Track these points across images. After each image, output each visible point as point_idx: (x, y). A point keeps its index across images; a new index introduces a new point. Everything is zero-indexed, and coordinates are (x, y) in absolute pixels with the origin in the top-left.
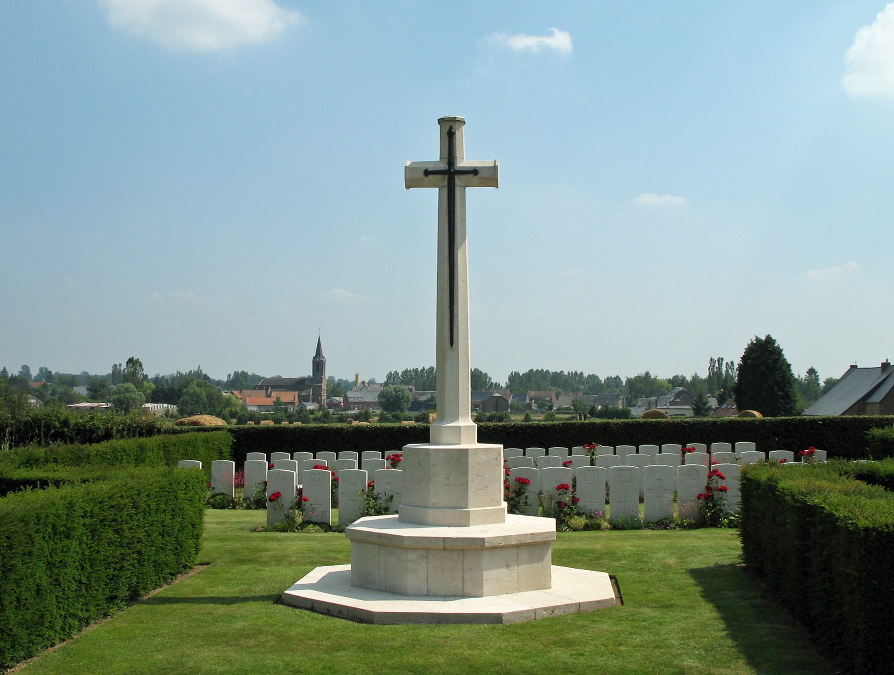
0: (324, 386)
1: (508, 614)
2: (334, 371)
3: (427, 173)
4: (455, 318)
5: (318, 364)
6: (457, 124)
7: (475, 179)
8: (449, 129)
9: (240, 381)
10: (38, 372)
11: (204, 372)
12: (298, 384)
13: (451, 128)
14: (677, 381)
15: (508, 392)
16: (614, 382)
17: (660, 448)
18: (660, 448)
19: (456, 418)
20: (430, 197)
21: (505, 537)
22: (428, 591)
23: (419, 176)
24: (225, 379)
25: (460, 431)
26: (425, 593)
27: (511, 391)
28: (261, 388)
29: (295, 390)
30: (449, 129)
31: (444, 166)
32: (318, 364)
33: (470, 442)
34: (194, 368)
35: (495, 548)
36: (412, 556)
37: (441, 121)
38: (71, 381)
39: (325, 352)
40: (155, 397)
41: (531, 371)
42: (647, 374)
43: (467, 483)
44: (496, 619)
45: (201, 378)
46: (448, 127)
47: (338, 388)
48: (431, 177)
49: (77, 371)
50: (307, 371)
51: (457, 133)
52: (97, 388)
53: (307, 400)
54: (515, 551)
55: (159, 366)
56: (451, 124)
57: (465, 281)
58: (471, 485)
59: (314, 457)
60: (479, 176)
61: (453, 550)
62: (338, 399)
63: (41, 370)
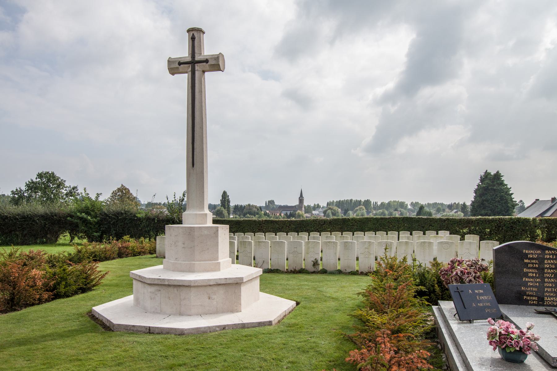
5: (301, 200)
30: (195, 35)
32: (301, 200)
48: (182, 66)
56: (193, 32)
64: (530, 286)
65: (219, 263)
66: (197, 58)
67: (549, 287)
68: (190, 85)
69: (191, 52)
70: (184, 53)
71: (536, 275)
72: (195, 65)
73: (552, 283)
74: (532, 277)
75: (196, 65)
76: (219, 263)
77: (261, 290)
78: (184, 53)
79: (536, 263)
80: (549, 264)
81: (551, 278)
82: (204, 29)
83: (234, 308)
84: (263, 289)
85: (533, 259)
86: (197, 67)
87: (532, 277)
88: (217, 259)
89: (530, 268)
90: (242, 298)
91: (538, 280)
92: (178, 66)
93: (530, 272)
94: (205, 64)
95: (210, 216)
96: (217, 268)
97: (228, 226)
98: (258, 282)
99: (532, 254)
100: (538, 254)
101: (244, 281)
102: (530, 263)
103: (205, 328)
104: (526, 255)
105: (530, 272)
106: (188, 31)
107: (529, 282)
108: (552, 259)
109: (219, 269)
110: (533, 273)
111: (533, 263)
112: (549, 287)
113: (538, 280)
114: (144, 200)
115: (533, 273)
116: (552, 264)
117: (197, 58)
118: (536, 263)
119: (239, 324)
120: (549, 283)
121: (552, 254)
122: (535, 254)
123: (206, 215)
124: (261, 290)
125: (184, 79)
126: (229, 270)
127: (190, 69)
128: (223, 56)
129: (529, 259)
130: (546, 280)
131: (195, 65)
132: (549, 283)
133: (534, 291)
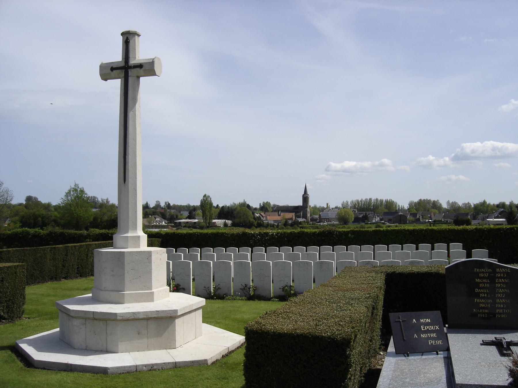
0: (308, 210)
1: (113, 368)
2: (312, 203)
3: (112, 69)
4: (127, 164)
5: (305, 199)
6: (131, 35)
7: (141, 71)
8: (128, 38)
9: (265, 208)
10: (408, 206)
11: (247, 203)
12: (295, 209)
13: (127, 39)
14: (502, 205)
15: (408, 212)
16: (468, 205)
17: (402, 247)
18: (402, 247)
19: (127, 232)
20: (115, 85)
21: (134, 313)
22: (86, 347)
23: (108, 72)
24: (258, 207)
25: (134, 238)
26: (85, 348)
27: (409, 212)
28: (275, 211)
29: (293, 212)
30: (128, 38)
31: (123, 64)
32: (305, 199)
33: (144, 247)
34: (242, 201)
35: (128, 320)
36: (76, 322)
37: (123, 34)
38: (179, 208)
39: (309, 192)
40: (219, 217)
41: (420, 200)
42: (484, 201)
43: (124, 274)
44: (103, 371)
45: (245, 206)
46: (126, 38)
47: (315, 210)
48: (114, 71)
49: (184, 203)
50: (299, 202)
51: (131, 41)
52: (192, 211)
53: (300, 217)
54: (145, 322)
55: (220, 200)
56: (127, 35)
57: (135, 140)
58: (127, 275)
59: (176, 252)
60: (143, 69)
61: (100, 320)
62: (316, 216)
63: (166, 203)
64: (482, 308)
65: (153, 293)
66: (132, 62)
67: (500, 308)
68: (123, 92)
69: (124, 57)
70: (117, 57)
71: (487, 295)
72: (128, 71)
73: (503, 303)
74: (484, 298)
75: (129, 70)
76: (153, 293)
77: (203, 322)
78: (117, 57)
79: (487, 283)
80: (500, 283)
81: (502, 298)
82: (139, 31)
83: (171, 345)
84: (207, 319)
85: (484, 278)
86: (131, 72)
87: (484, 298)
88: (150, 288)
89: (481, 288)
90: (177, 333)
91: (489, 301)
92: (110, 71)
93: (482, 293)
94: (138, 69)
95: (144, 237)
96: (150, 297)
97: (301, 204)
98: (200, 312)
99: (483, 272)
100: (489, 273)
101: (179, 314)
102: (481, 283)
103: (130, 367)
104: (478, 273)
105: (482, 293)
106: (123, 34)
107: (481, 303)
108: (504, 278)
109: (152, 300)
110: (484, 293)
111: (484, 283)
112: (500, 308)
113: (489, 301)
114: (100, 200)
115: (484, 293)
116: (503, 283)
117: (132, 62)
118: (487, 283)
119: (169, 363)
120: (500, 303)
121: (503, 273)
122: (486, 273)
123: (139, 237)
124: (203, 322)
125: (115, 85)
126: (166, 300)
127: (123, 75)
128: (159, 59)
129: (481, 278)
130: (498, 300)
131: (128, 71)
132: (500, 303)
133: (486, 313)
